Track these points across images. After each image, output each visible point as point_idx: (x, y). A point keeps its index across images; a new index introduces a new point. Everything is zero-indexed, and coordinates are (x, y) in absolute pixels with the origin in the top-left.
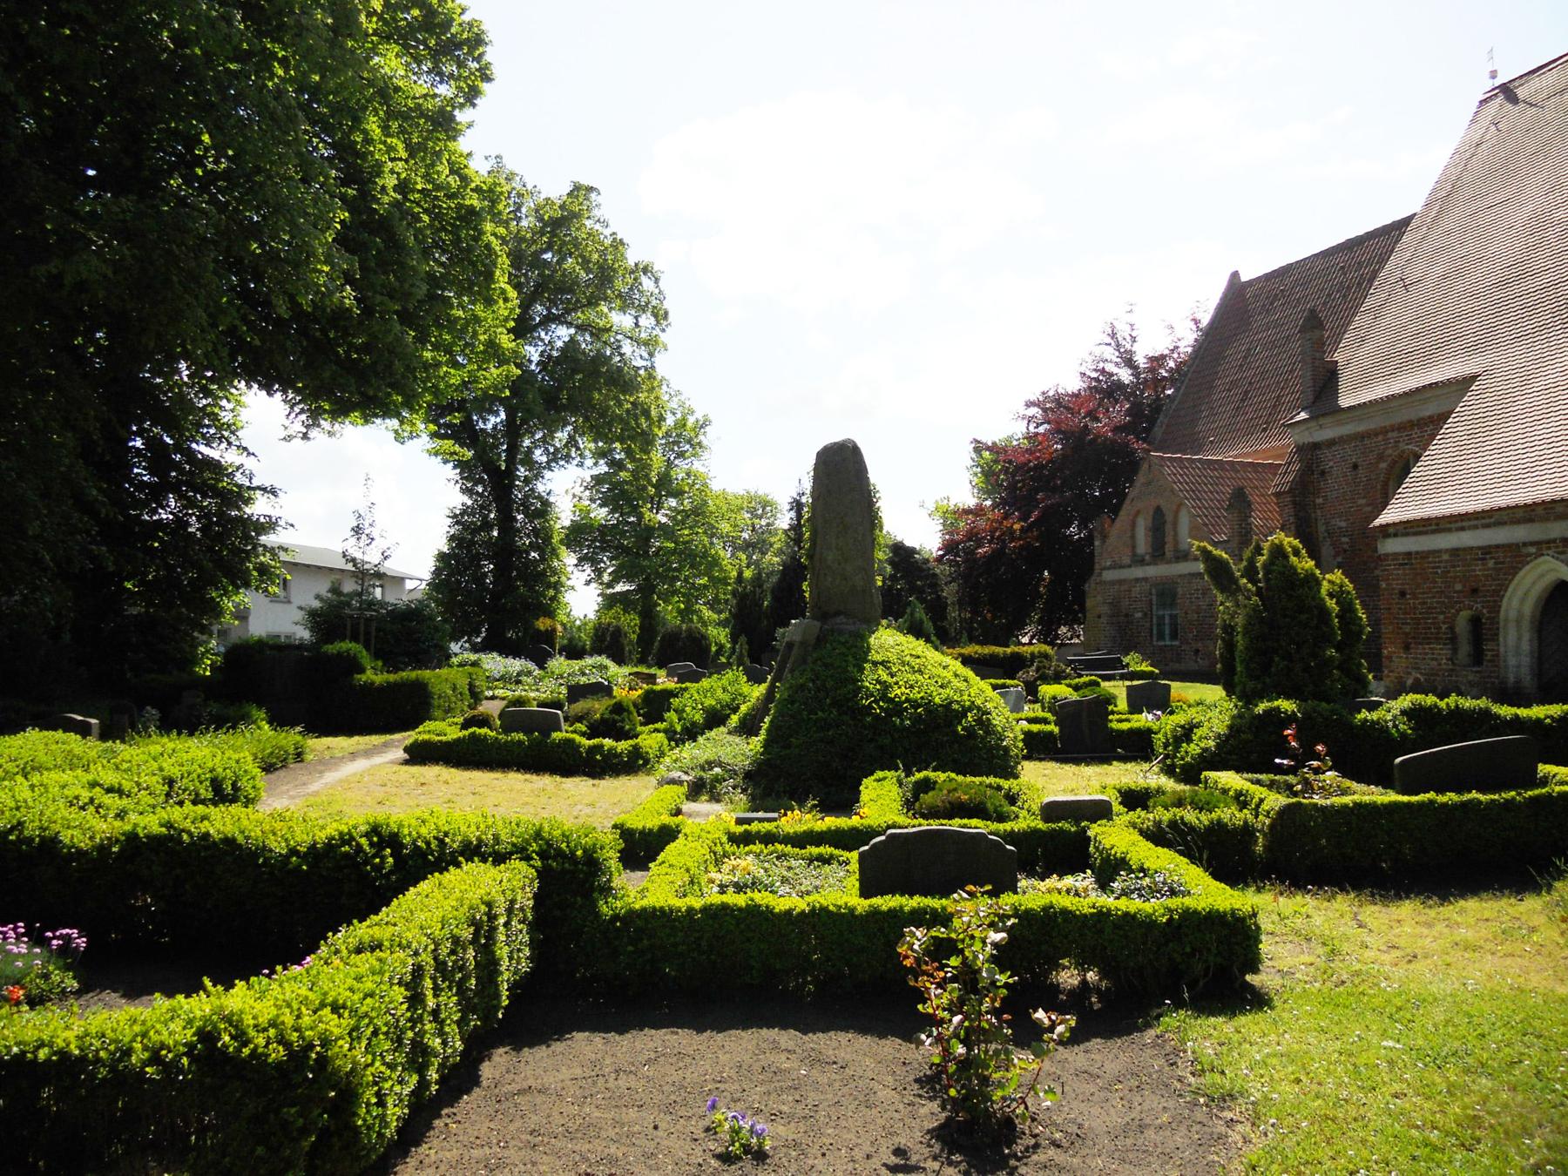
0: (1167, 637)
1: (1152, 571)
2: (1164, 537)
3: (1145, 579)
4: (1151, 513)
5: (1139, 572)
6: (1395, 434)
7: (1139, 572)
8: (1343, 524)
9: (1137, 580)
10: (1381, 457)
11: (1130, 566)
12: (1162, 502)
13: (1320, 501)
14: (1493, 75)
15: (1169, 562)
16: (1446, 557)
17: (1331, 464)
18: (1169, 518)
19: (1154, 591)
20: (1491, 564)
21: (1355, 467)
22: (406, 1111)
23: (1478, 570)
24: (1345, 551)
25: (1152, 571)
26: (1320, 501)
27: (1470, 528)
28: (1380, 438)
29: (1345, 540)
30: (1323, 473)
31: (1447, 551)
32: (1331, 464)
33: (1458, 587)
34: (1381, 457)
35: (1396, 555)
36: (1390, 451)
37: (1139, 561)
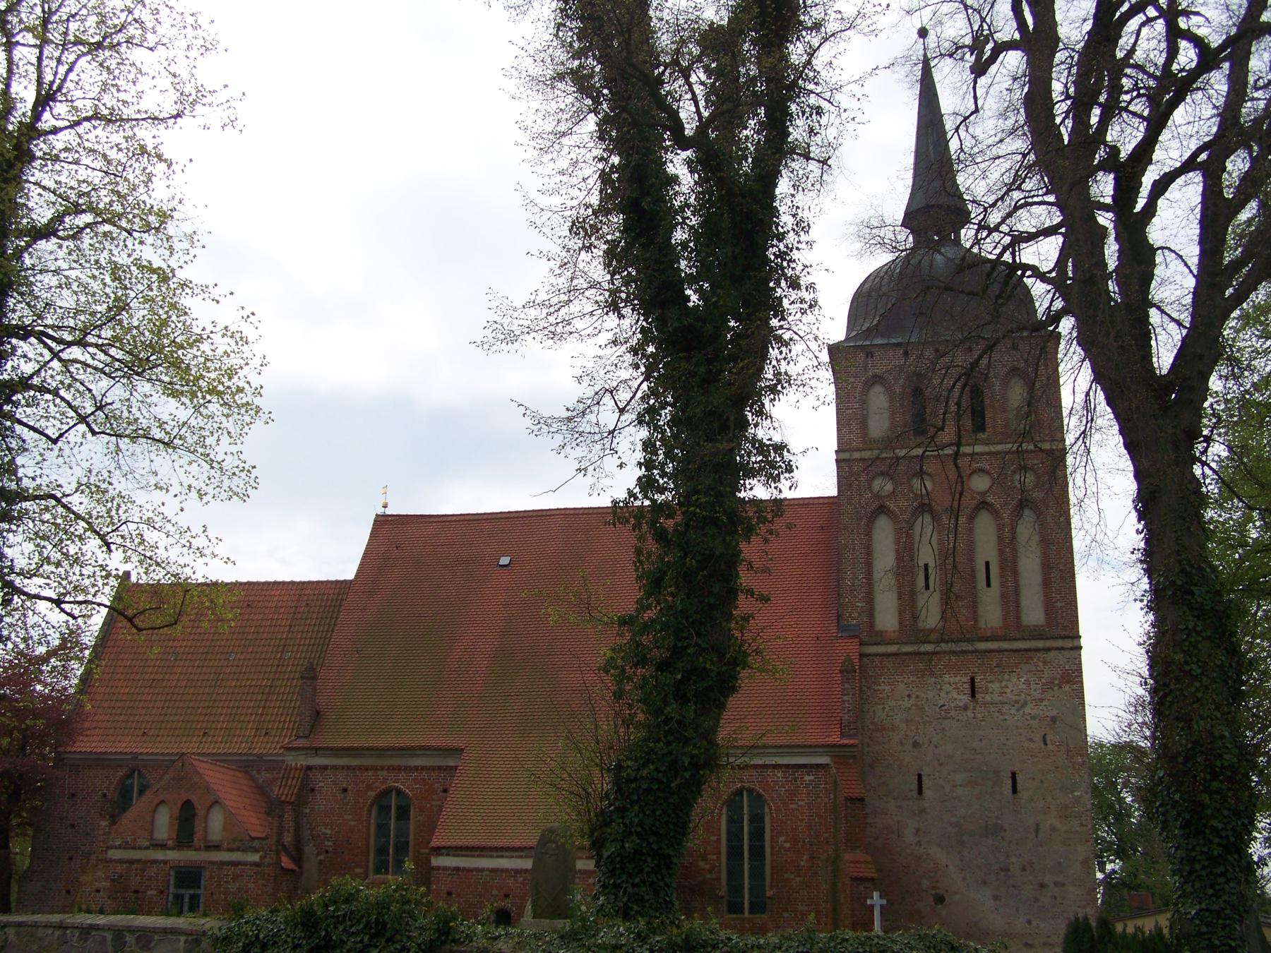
0: (186, 899)
1: (172, 855)
2: (193, 827)
3: (165, 862)
4: (179, 805)
5: (159, 855)
6: (385, 773)
7: (159, 855)
8: (328, 831)
9: (155, 862)
10: (369, 787)
11: (147, 848)
12: (193, 798)
13: (308, 811)
14: (385, 506)
15: (199, 849)
16: (487, 873)
17: (322, 784)
18: (201, 812)
19: (172, 873)
20: (521, 879)
21: (345, 790)
22: (743, 70)
23: (511, 882)
24: (327, 852)
25: (172, 855)
26: (308, 811)
27: (507, 857)
28: (370, 773)
29: (330, 844)
30: (313, 790)
31: (488, 869)
32: (322, 784)
33: (495, 892)
34: (369, 787)
35: (445, 869)
36: (377, 784)
37: (163, 846)
